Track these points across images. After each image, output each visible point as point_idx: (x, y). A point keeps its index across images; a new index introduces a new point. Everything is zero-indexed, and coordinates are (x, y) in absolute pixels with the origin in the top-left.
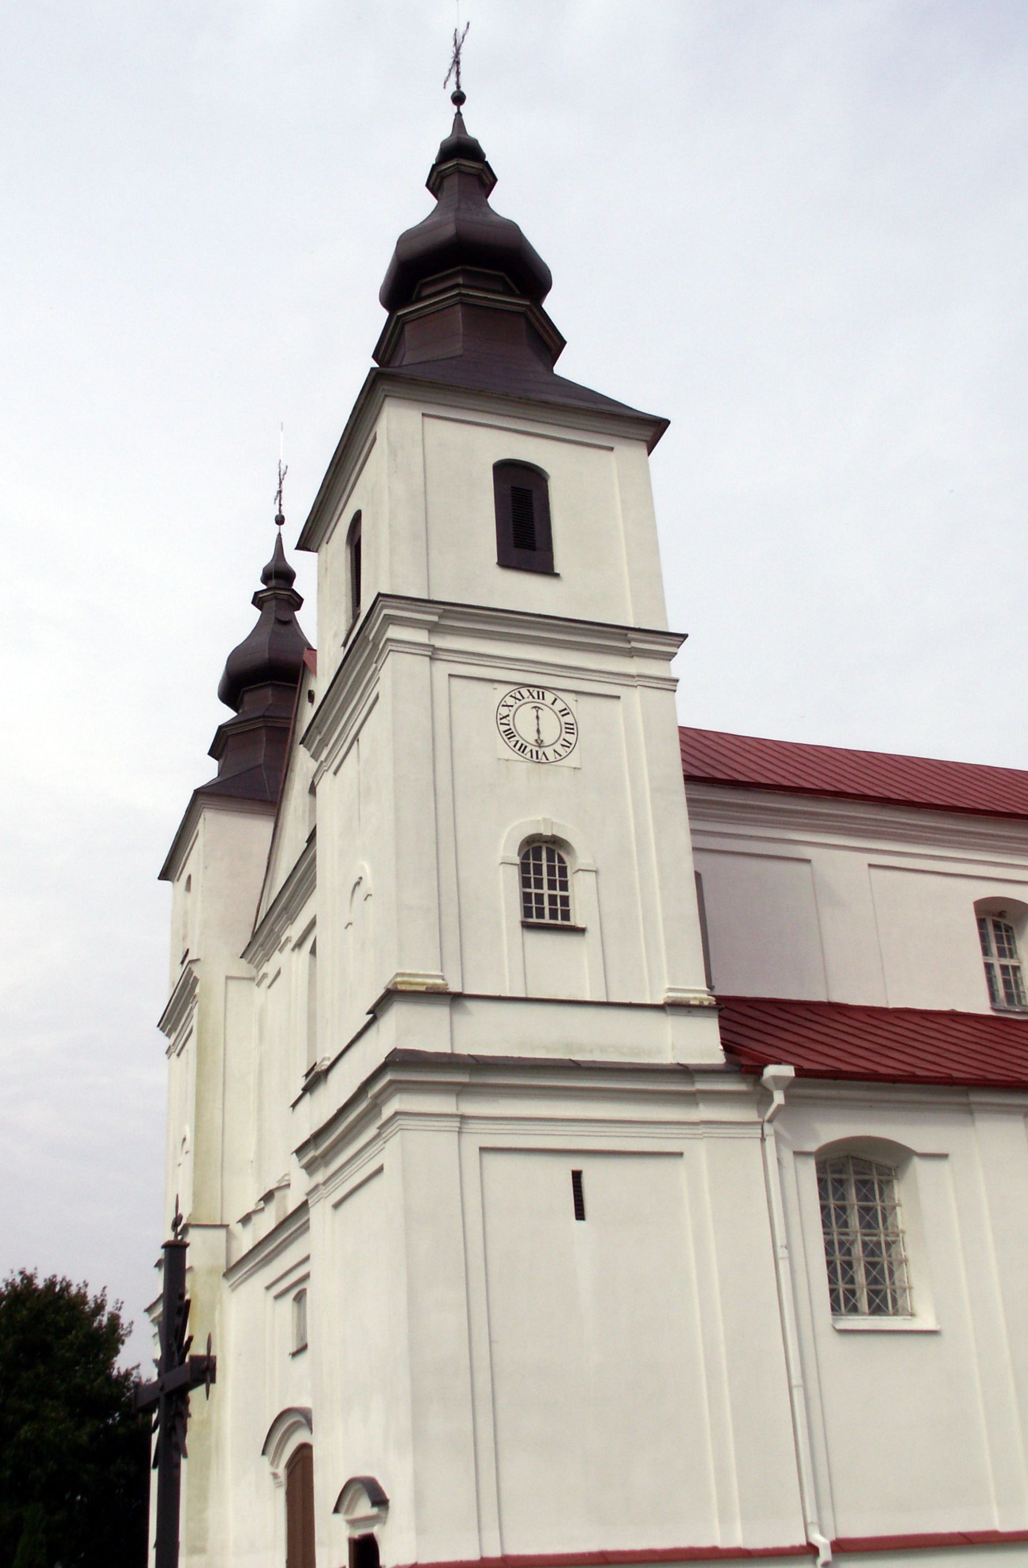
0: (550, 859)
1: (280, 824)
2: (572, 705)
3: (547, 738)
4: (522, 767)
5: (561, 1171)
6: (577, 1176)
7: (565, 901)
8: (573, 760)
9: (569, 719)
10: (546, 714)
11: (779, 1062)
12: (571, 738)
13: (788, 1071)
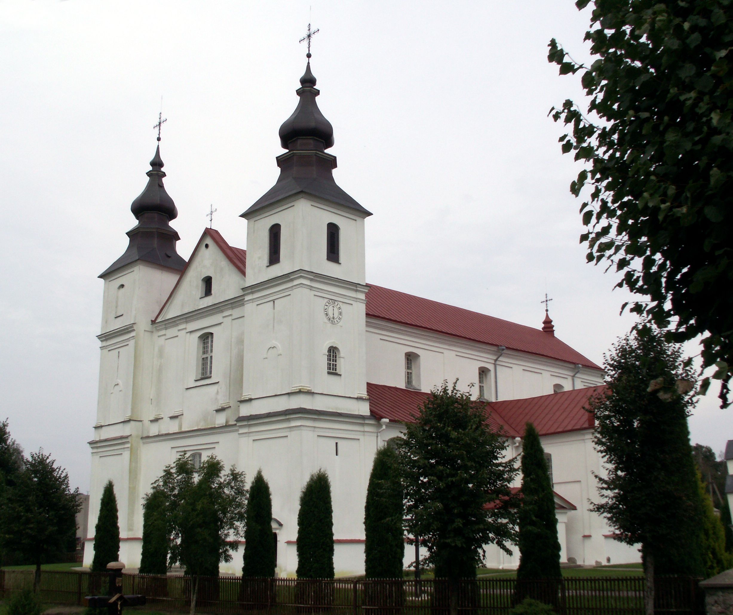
0: (333, 353)
1: (180, 283)
2: (342, 307)
3: (336, 316)
4: (329, 325)
5: (333, 442)
6: (337, 443)
7: (336, 365)
8: (340, 324)
9: (340, 311)
10: (335, 309)
11: (385, 418)
12: (340, 316)
13: (387, 420)
